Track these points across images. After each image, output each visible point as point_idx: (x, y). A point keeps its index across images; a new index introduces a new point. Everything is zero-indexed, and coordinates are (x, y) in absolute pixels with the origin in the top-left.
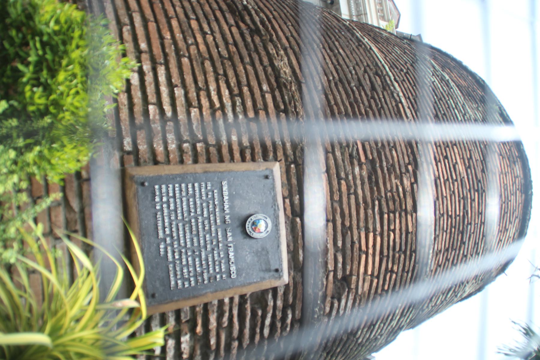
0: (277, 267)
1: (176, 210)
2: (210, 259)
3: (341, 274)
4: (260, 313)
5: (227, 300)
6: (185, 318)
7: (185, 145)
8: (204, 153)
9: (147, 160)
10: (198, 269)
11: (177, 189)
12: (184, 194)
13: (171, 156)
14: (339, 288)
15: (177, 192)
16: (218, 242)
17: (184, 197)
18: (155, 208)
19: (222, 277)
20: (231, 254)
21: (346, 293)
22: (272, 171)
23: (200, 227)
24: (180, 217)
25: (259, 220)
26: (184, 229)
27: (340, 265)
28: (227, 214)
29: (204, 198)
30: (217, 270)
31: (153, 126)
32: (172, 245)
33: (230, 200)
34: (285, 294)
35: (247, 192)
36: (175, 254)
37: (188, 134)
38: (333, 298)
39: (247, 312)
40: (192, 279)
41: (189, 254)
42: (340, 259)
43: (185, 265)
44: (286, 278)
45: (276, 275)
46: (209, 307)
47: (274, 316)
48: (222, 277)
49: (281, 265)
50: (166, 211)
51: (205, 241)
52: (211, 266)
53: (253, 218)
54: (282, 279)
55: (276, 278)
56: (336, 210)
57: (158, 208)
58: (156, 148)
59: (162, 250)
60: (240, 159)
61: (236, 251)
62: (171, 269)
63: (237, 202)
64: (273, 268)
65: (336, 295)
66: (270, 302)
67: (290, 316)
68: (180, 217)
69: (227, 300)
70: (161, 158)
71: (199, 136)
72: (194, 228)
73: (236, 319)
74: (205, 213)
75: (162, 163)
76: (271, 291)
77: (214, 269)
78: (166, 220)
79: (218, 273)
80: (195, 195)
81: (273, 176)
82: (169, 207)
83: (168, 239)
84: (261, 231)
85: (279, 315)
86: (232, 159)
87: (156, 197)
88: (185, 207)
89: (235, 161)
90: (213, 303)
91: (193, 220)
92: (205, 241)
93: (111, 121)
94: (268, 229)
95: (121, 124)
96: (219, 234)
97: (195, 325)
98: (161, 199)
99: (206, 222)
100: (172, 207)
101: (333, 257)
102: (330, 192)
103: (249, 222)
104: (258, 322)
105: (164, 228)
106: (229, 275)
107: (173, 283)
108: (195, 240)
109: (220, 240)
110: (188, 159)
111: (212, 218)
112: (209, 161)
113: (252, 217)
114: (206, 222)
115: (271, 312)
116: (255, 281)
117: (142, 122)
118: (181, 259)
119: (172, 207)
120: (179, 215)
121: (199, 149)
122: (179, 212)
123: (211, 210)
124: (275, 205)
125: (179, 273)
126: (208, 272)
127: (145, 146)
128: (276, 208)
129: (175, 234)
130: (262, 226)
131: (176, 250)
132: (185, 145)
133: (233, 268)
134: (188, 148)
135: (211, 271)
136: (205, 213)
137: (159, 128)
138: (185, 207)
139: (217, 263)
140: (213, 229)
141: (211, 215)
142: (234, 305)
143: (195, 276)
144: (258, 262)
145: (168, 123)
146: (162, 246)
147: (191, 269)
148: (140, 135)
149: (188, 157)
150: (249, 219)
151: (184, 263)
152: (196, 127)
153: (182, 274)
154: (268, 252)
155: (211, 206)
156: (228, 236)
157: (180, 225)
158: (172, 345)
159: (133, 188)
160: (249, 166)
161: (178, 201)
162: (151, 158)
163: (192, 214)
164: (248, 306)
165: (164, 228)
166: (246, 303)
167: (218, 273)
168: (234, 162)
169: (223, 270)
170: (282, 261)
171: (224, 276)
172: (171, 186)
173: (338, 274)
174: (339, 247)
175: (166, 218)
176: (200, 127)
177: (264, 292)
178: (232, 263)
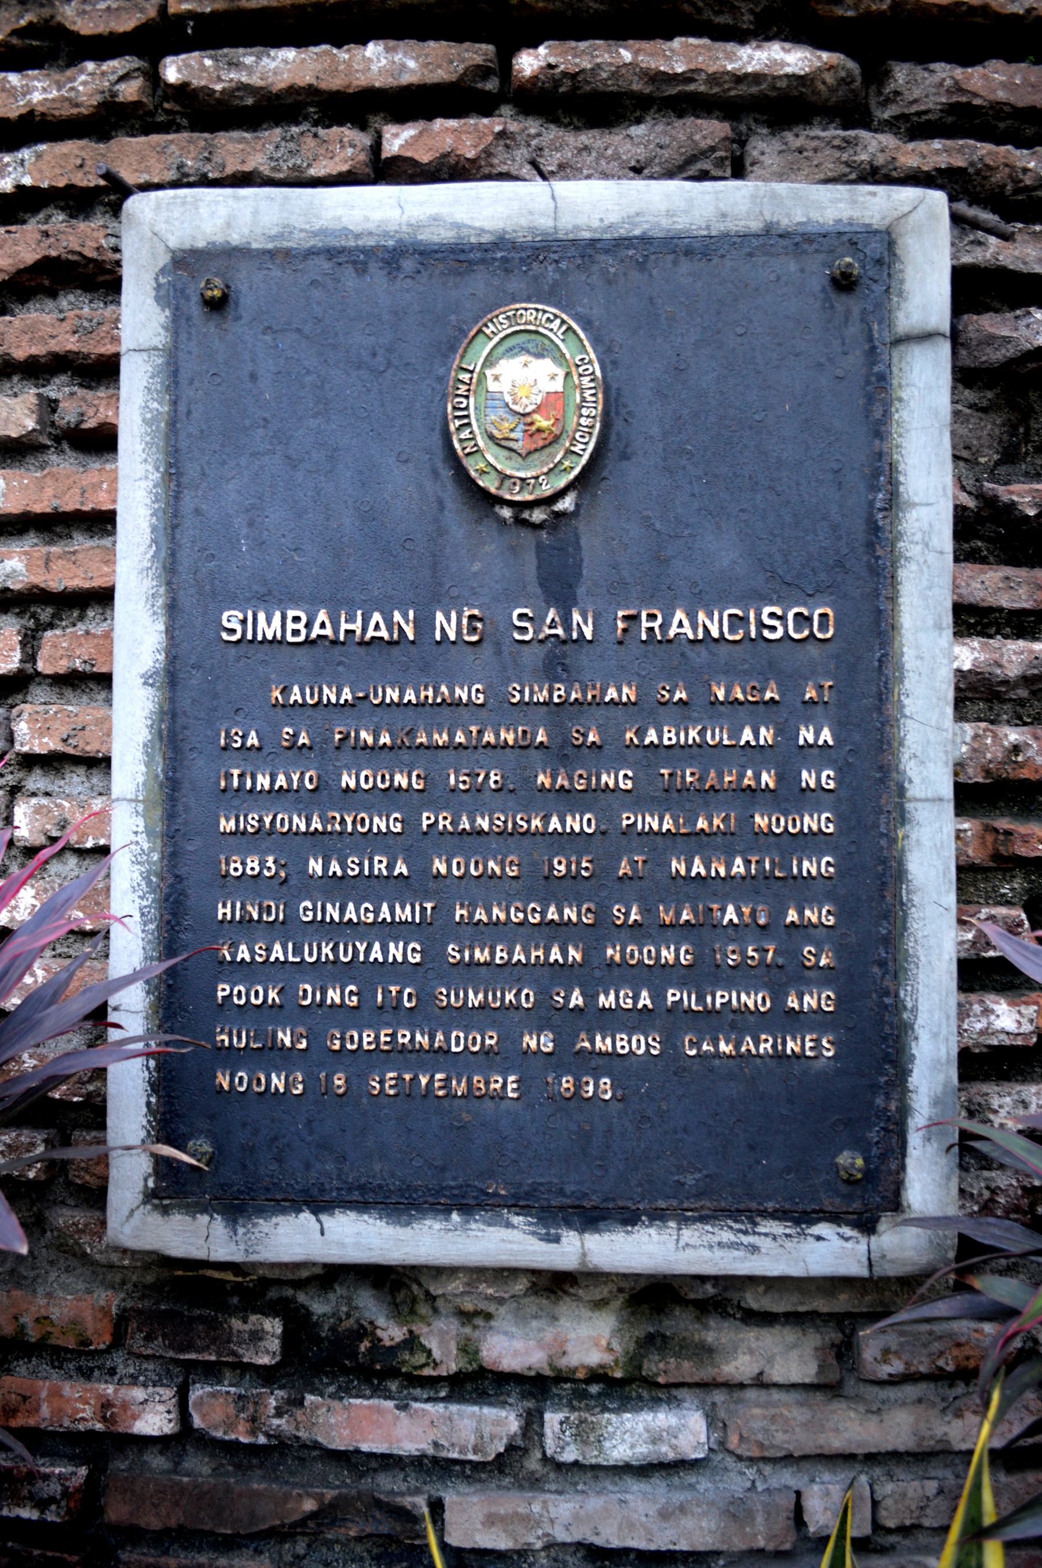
22: (186, 262)
118: (659, 976)
171: (806, 735)
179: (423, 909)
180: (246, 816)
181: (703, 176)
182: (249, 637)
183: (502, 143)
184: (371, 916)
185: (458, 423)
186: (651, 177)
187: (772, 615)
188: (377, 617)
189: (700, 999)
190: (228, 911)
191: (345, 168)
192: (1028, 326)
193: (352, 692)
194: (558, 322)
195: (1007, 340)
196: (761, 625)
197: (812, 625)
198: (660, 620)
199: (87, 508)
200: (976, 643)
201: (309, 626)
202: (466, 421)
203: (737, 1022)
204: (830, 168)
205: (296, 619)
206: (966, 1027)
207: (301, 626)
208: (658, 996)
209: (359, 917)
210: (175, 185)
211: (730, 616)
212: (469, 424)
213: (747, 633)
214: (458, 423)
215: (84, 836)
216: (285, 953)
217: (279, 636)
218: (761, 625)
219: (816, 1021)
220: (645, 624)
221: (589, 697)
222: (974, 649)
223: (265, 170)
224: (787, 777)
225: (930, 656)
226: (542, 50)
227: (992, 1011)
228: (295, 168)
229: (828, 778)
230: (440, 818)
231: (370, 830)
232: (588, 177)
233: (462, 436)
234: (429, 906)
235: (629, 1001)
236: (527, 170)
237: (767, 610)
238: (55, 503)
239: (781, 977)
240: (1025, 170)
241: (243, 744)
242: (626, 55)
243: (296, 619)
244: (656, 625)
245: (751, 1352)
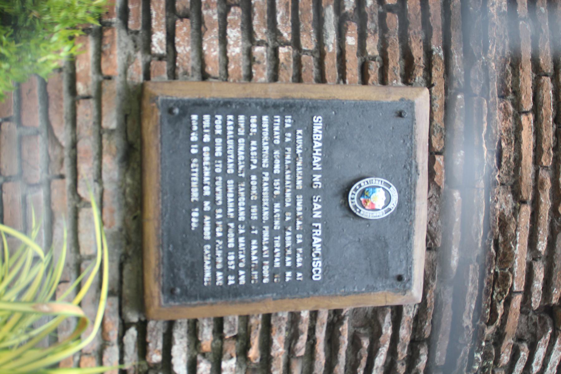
0: (401, 272)
2: (277, 244)
3: (539, 301)
4: (366, 343)
5: (305, 315)
6: (230, 332)
7: (258, 50)
8: (292, 66)
9: (190, 71)
10: (254, 258)
11: (229, 123)
12: (241, 132)
13: (232, 67)
14: (535, 324)
15: (230, 128)
16: (295, 217)
17: (241, 137)
18: (190, 151)
19: (294, 276)
20: (317, 241)
21: (548, 337)
22: (412, 105)
23: (266, 189)
24: (230, 171)
25: (374, 187)
26: (236, 190)
27: (538, 285)
28: (317, 172)
29: (277, 142)
30: (288, 264)
31: (204, 12)
32: (212, 214)
33: (325, 149)
34: (418, 319)
35: (360, 137)
36: (218, 229)
37: (264, 30)
38: (520, 339)
39: (341, 338)
40: (241, 272)
41: (241, 231)
42: (540, 274)
43: (231, 250)
44: (416, 292)
45: (399, 285)
46: (272, 321)
47: (392, 352)
48: (294, 276)
49: (409, 269)
50: (207, 157)
51: (272, 214)
52: (278, 255)
53: (363, 183)
54: (408, 293)
55: (397, 291)
56: (542, 183)
57: (194, 151)
58: (206, 53)
59: (194, 220)
60: (358, 78)
61: (326, 236)
62: (207, 252)
63: (339, 154)
64: (393, 273)
65: (527, 337)
66: (387, 329)
67: (424, 358)
68: (230, 171)
69: (305, 315)
70: (212, 69)
71: (285, 35)
72: (254, 191)
73: (320, 347)
74: (277, 167)
75: (215, 78)
76: (390, 310)
77: (283, 262)
78: (207, 173)
79: (289, 269)
80: (261, 135)
81: (413, 113)
82: (213, 151)
83: (207, 206)
84: (377, 207)
85: (403, 352)
86: (342, 75)
87: (193, 134)
88: (241, 154)
89: (347, 81)
90: (280, 315)
91: (254, 177)
92: (272, 214)
94: (390, 206)
95: (152, 8)
96: (299, 204)
97: (246, 347)
98: (201, 137)
99: (277, 182)
100: (219, 152)
101: (524, 268)
102: (535, 150)
103: (356, 190)
104: (361, 357)
105: (201, 185)
106: (309, 274)
107: (208, 274)
108: (254, 209)
109: (299, 214)
110: (262, 74)
111: (288, 177)
112: (298, 78)
113: (361, 182)
114: (277, 182)
115: (387, 345)
116: (356, 290)
117: (188, 6)
118: (225, 238)
119: (219, 152)
120: (231, 166)
121: (281, 57)
122: (230, 161)
123: (287, 162)
124: (411, 164)
125: (219, 260)
126: (272, 264)
127: (188, 48)
128: (413, 171)
129: (219, 197)
131: (219, 223)
132: (258, 50)
133: (317, 264)
134: (263, 55)
135: (277, 265)
136: (277, 167)
137: (216, 17)
138: (241, 154)
139: (289, 252)
140: (288, 195)
141: (288, 172)
142: (318, 324)
143: (248, 268)
144: (366, 259)
145: (232, 9)
146: (195, 214)
147: (241, 256)
148: (181, 29)
149: (261, 71)
150: (356, 185)
151: (231, 245)
152: (282, 18)
153: (225, 261)
154: (387, 246)
155: (288, 157)
156: (315, 209)
157: (230, 182)
158: (206, 370)
159: (154, 116)
160: (372, 93)
161: (230, 143)
162: (198, 68)
163: (253, 167)
164: (345, 330)
165: (201, 185)
166: (342, 324)
167: (289, 269)
168: (345, 82)
169: (299, 265)
170: (411, 263)
171: (299, 274)
172: (219, 117)
173: (533, 299)
174: (540, 252)
175: (206, 169)
176: (290, 17)
177: (378, 311)
178: (317, 255)
181: (427, 240)
186: (427, 226)
191: (433, 146)
195: (384, 320)
199: (347, 71)
200: (308, 317)
201: (317, 141)
204: (428, 272)
210: (431, 97)
215: (256, 69)
219: (226, 281)
221: (316, 225)
223: (434, 123)
226: (459, 198)
228: (434, 132)
229: (231, 282)
232: (428, 209)
236: (431, 193)
238: (348, 61)
239: (226, 271)
240: (426, 323)
242: (457, 220)
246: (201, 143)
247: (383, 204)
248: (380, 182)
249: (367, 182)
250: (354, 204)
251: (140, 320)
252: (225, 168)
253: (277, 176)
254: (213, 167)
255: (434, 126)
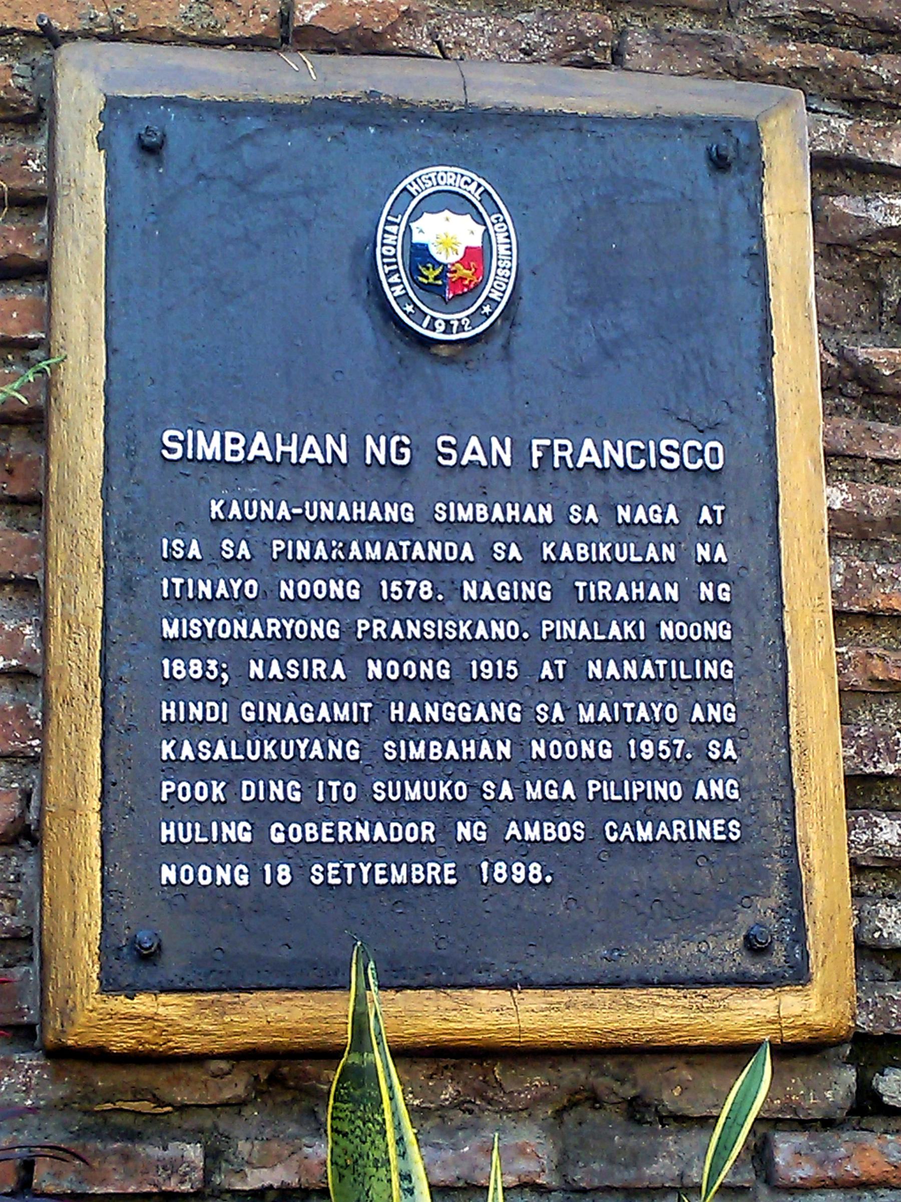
1: (303, 770)
28: (357, 448)
49: (795, 908)
82: (285, 811)
93: (780, 1172)
94: (472, 193)
98: (231, 852)
118: (581, 770)
130: (447, 235)
133: (672, 451)
179: (361, 710)
180: (188, 622)
182: (190, 456)
183: (406, 20)
184: (311, 716)
185: (387, 269)
187: (670, 448)
188: (311, 440)
189: (620, 790)
190: (172, 711)
192: (876, 208)
193: (290, 510)
194: (475, 185)
196: (659, 456)
197: (703, 458)
198: (570, 450)
201: (247, 448)
202: (395, 267)
203: (653, 810)
205: (235, 441)
206: (852, 838)
207: (239, 447)
208: (581, 787)
209: (299, 716)
211: (633, 447)
212: (397, 271)
213: (648, 463)
214: (387, 269)
216: (229, 752)
217: (218, 457)
218: (659, 456)
220: (557, 453)
222: (842, 491)
224: (688, 591)
225: (807, 497)
227: (876, 824)
230: (375, 625)
231: (326, 622)
233: (391, 280)
234: (366, 706)
235: (555, 792)
237: (664, 443)
241: (185, 555)
243: (235, 441)
244: (567, 454)
245: (670, 1155)
246: (255, 854)
247: (467, 221)
248: (393, 229)
249: (388, 275)
250: (466, 322)
251: (851, 1060)
252: (341, 768)
253: (370, 589)
254: (339, 809)
255: (191, 28)
